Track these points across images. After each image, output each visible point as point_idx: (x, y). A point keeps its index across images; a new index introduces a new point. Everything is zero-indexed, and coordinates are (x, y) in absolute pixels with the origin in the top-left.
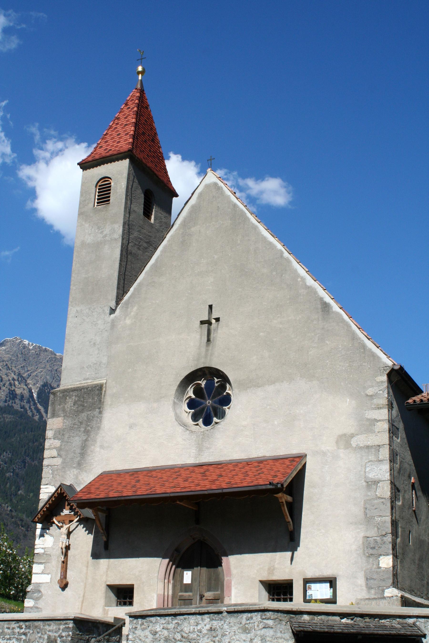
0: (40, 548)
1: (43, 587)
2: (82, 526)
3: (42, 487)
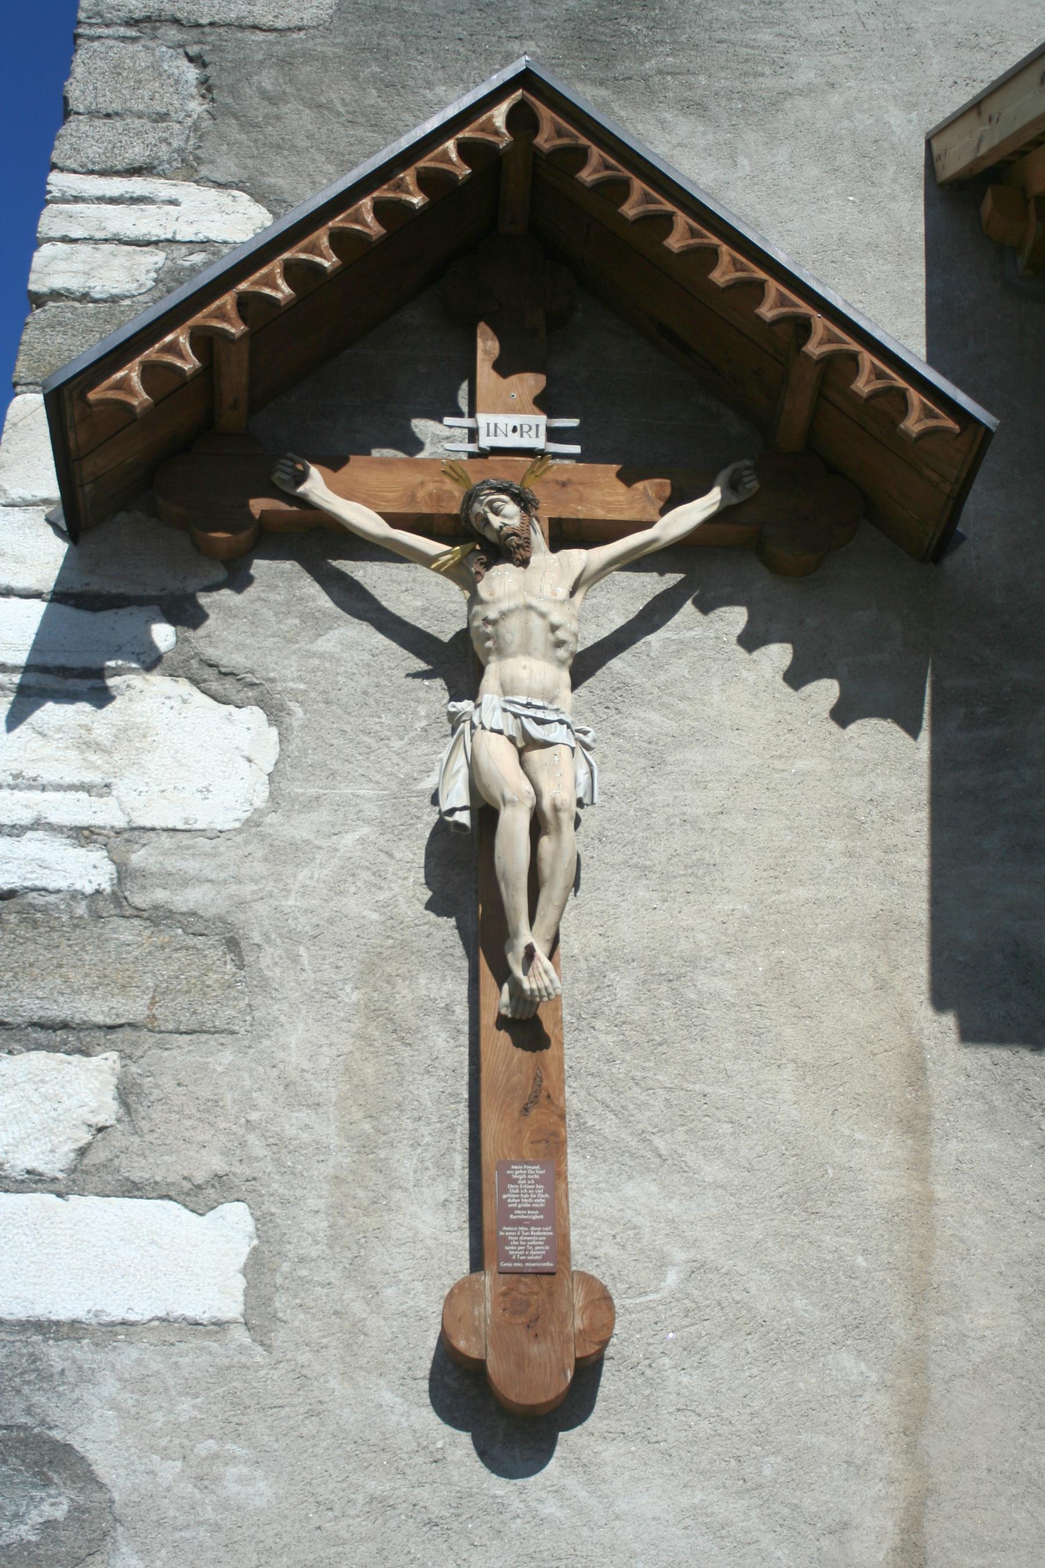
0: (37, 825)
1: (109, 1387)
2: (736, 617)
3: (58, 182)
